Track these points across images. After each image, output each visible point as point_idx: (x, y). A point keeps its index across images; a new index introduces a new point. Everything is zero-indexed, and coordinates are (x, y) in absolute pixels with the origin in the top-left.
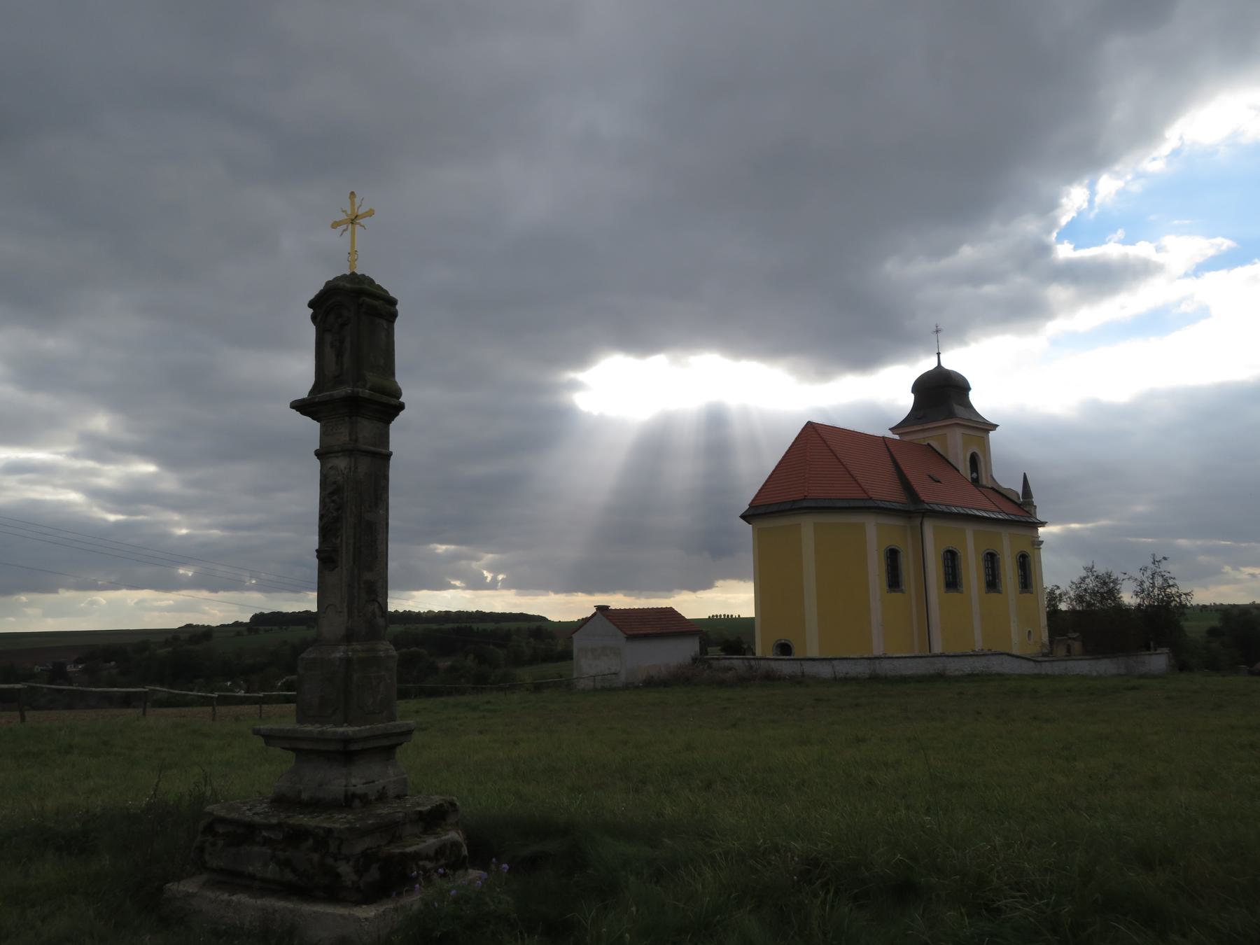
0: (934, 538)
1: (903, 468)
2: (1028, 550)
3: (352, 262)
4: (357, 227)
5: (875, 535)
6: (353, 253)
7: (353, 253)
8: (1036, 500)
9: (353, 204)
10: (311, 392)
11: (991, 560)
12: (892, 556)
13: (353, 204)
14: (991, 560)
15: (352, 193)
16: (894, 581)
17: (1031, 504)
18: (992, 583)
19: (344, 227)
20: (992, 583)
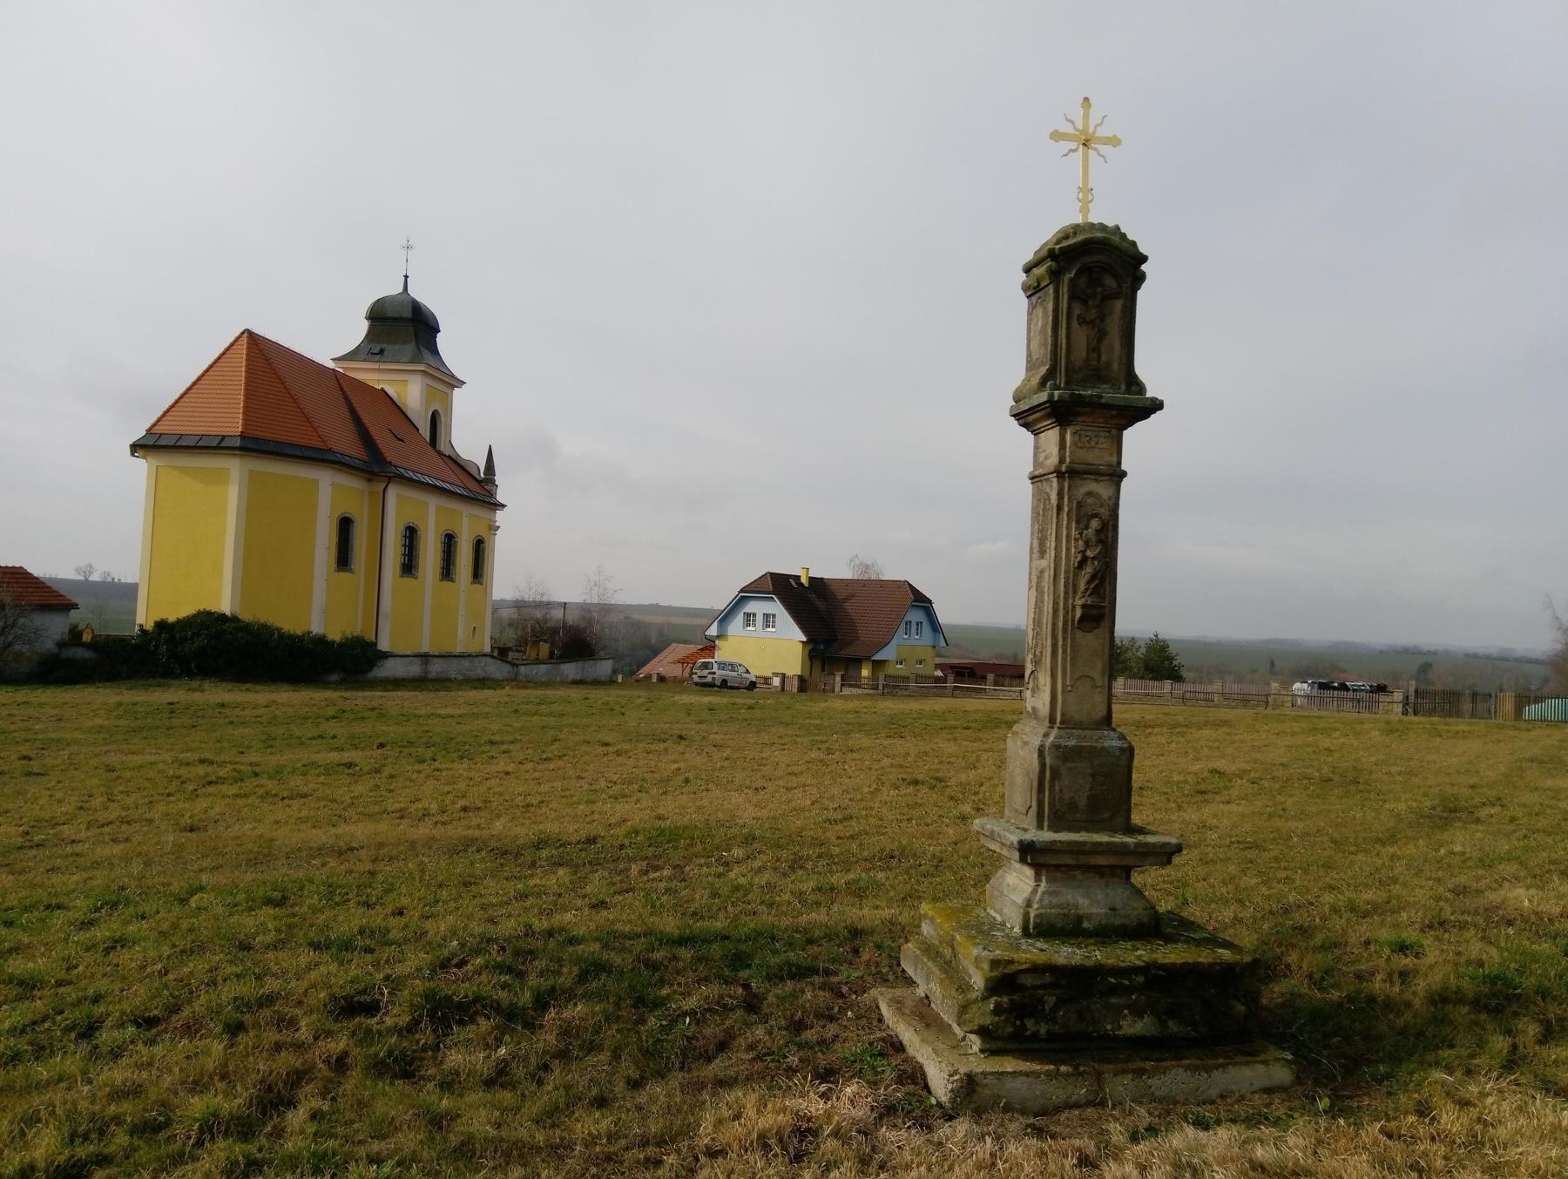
0: (399, 505)
1: (373, 430)
2: (485, 535)
3: (1085, 210)
4: (1091, 153)
5: (330, 493)
6: (1086, 191)
7: (1086, 191)
8: (498, 479)
9: (1086, 116)
10: (179, 621)
11: (449, 541)
12: (345, 525)
13: (1086, 116)
14: (449, 541)
15: (1086, 99)
16: (344, 560)
17: (492, 482)
18: (447, 572)
19: (1073, 145)
20: (447, 572)
